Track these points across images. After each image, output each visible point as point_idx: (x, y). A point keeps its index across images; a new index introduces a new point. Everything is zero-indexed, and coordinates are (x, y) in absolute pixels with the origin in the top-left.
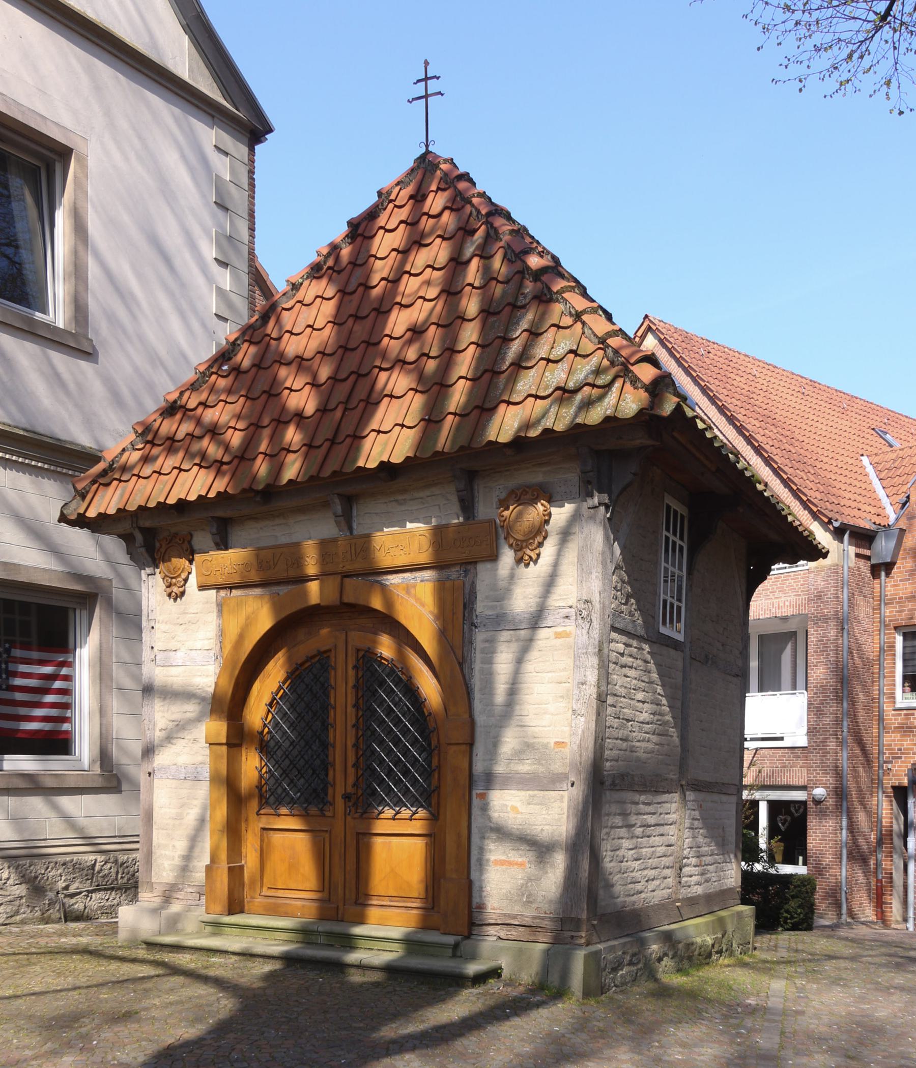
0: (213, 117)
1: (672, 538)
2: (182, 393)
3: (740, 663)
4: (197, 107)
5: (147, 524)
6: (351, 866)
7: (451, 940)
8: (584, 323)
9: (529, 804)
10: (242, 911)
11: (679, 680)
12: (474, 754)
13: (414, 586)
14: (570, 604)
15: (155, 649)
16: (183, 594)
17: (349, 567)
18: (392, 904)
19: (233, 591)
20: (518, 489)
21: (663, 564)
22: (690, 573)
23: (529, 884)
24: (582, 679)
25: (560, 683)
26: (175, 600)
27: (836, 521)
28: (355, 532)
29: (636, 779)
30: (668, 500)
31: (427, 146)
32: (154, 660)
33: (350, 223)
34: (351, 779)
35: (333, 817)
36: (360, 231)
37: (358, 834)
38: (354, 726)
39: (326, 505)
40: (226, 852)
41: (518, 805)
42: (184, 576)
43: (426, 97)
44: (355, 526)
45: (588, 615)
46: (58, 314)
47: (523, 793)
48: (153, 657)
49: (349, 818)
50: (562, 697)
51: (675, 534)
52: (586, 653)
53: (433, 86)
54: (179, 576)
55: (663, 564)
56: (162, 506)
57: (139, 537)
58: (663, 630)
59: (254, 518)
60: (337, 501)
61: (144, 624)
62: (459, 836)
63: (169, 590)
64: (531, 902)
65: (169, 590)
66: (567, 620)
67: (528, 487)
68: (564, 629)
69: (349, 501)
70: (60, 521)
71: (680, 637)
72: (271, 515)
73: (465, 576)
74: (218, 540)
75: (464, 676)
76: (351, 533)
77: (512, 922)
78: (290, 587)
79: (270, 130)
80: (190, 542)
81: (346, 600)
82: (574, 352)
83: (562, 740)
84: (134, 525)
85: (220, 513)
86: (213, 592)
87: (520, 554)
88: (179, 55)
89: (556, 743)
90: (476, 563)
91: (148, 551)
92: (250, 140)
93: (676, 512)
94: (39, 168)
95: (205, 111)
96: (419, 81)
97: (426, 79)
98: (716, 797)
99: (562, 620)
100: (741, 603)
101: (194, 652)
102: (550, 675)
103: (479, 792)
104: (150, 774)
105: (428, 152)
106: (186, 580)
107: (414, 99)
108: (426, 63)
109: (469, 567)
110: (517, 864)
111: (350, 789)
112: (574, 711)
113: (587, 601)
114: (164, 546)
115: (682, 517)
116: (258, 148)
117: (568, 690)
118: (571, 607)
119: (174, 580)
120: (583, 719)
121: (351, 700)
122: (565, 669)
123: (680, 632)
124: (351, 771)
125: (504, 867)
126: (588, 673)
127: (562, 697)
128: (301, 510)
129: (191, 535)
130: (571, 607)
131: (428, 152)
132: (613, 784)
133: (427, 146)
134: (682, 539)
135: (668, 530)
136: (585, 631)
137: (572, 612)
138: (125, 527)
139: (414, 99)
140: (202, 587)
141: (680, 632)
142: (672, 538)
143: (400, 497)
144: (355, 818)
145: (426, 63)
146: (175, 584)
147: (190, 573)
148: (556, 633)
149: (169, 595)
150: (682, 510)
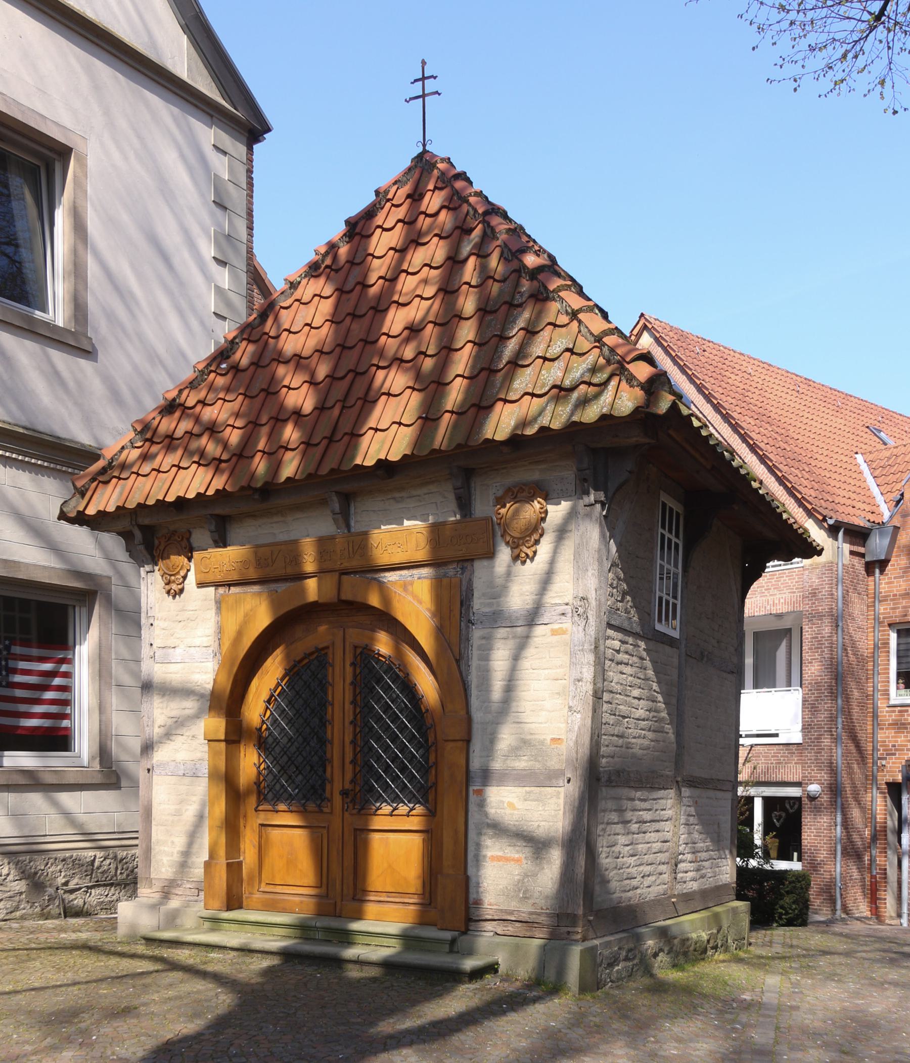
0: (212, 116)
1: (667, 535)
2: (181, 391)
5: (146, 521)
6: (349, 861)
7: (448, 935)
8: (580, 322)
9: (526, 800)
10: (240, 907)
13: (412, 583)
14: (566, 601)
15: (154, 646)
16: (181, 591)
17: (346, 565)
20: (514, 487)
21: (659, 561)
22: (685, 570)
23: (526, 880)
24: (578, 676)
26: (174, 597)
28: (353, 530)
29: (632, 775)
30: (664, 497)
31: (424, 145)
32: (153, 657)
33: (347, 222)
34: (349, 775)
35: (331, 813)
36: (357, 230)
37: (356, 830)
39: (324, 503)
43: (423, 96)
44: (352, 524)
45: (584, 612)
47: (520, 789)
48: (152, 654)
50: (558, 694)
52: (583, 650)
53: (430, 86)
54: (178, 573)
55: (659, 561)
56: (161, 503)
57: (138, 534)
58: (659, 627)
59: (252, 515)
60: (335, 498)
63: (168, 587)
65: (168, 587)
66: (563, 617)
67: (525, 484)
68: (561, 625)
69: (347, 499)
70: (59, 519)
71: (676, 634)
73: (462, 574)
74: (217, 538)
76: (349, 531)
78: (288, 584)
79: (268, 130)
80: (188, 540)
81: (343, 597)
82: (570, 350)
84: (134, 523)
85: (219, 511)
86: (213, 589)
87: (516, 551)
89: (553, 739)
90: (472, 560)
92: (248, 139)
93: (671, 510)
95: (203, 111)
96: (416, 81)
97: (424, 78)
98: (711, 793)
99: (559, 617)
102: (546, 671)
103: (475, 788)
104: (149, 770)
106: (185, 577)
107: (411, 99)
108: (424, 63)
109: (466, 564)
110: (513, 860)
111: (347, 786)
112: (570, 707)
113: (583, 599)
115: (678, 514)
118: (567, 604)
119: (173, 578)
120: (579, 716)
121: (349, 696)
122: (561, 666)
124: (349, 768)
126: (584, 670)
127: (558, 694)
129: (190, 533)
130: (567, 604)
131: (425, 151)
133: (424, 145)
134: (677, 536)
135: (663, 527)
136: (581, 628)
137: (568, 609)
138: (125, 524)
140: (201, 585)
142: (667, 535)
143: (397, 495)
145: (424, 63)
146: (174, 582)
147: (188, 570)
148: (552, 630)
149: (168, 592)
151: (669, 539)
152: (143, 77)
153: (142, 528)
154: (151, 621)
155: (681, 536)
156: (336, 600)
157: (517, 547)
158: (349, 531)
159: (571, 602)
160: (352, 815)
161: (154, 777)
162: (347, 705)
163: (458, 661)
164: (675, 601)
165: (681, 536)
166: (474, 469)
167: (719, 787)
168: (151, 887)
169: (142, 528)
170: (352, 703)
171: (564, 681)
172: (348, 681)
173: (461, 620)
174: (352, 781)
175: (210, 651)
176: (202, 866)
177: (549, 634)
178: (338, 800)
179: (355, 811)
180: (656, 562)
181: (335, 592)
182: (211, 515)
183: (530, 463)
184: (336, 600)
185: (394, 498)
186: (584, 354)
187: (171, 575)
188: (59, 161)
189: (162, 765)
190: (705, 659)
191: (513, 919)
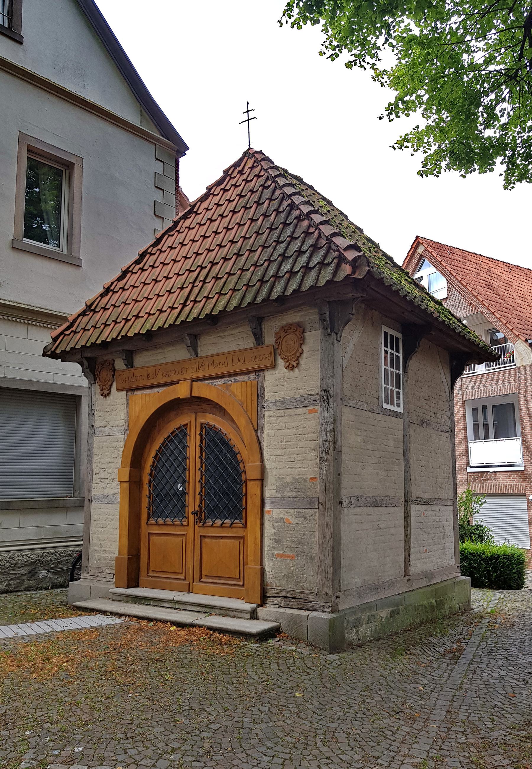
1: (390, 351)
2: (112, 283)
3: (449, 424)
5: (89, 355)
6: (197, 557)
7: (249, 607)
8: (320, 229)
10: (137, 586)
11: (401, 436)
12: (264, 486)
13: (231, 385)
14: (317, 392)
15: (95, 426)
16: (109, 394)
17: (195, 376)
18: (220, 581)
20: (286, 326)
21: (383, 367)
22: (405, 371)
23: (297, 570)
25: (313, 441)
27: (530, 339)
28: (199, 356)
29: (368, 500)
30: (385, 329)
31: (249, 145)
33: (207, 188)
34: (198, 502)
35: (188, 526)
36: (212, 192)
37: (201, 536)
38: (199, 469)
39: (182, 340)
41: (290, 518)
42: (110, 383)
44: (199, 352)
45: (327, 399)
48: (93, 431)
49: (196, 526)
50: (314, 449)
51: (392, 348)
53: (251, 115)
55: (383, 367)
56: (93, 345)
57: (86, 363)
58: (385, 406)
59: (146, 349)
60: (187, 338)
62: (255, 538)
64: (299, 582)
65: (102, 392)
66: (315, 402)
67: (291, 325)
68: (314, 407)
69: (195, 337)
71: (400, 410)
72: (155, 347)
73: (258, 378)
74: (127, 363)
75: (258, 437)
76: (197, 356)
77: (288, 595)
78: (165, 388)
79: (188, 149)
80: (113, 365)
81: (193, 395)
83: (314, 477)
85: (126, 347)
86: (125, 392)
87: (288, 364)
88: (130, 113)
89: (311, 478)
90: (264, 370)
91: (90, 371)
93: (392, 336)
97: (248, 111)
98: (436, 508)
99: (312, 402)
100: (447, 388)
101: (114, 427)
104: (89, 500)
105: (250, 148)
109: (261, 373)
110: (290, 557)
111: (197, 509)
114: (100, 367)
115: (397, 339)
117: (317, 445)
121: (198, 454)
122: (315, 432)
123: (400, 406)
124: (198, 497)
125: (282, 558)
127: (314, 449)
128: (171, 344)
129: (114, 361)
130: (317, 394)
131: (250, 148)
132: (350, 503)
133: (249, 145)
134: (398, 351)
135: (386, 346)
136: (325, 409)
137: (318, 397)
138: (78, 356)
140: (119, 390)
141: (400, 406)
142: (390, 351)
143: (222, 334)
144: (199, 527)
147: (112, 382)
150: (397, 334)
151: (398, 352)
153: (87, 359)
154: (93, 412)
155: (401, 351)
156: (189, 396)
157: (288, 361)
158: (197, 356)
160: (199, 527)
161: (92, 504)
162: (197, 457)
163: (256, 431)
164: (398, 390)
165: (401, 351)
166: (264, 317)
167: (441, 504)
168: (88, 573)
169: (87, 359)
170: (200, 457)
172: (198, 444)
173: (258, 406)
174: (199, 506)
175: (123, 429)
176: (115, 559)
177: (308, 413)
178: (191, 517)
179: (201, 524)
180: (381, 367)
181: (189, 392)
182: (123, 350)
183: (294, 312)
184: (189, 396)
187: (103, 386)
189: (98, 497)
190: (425, 424)
191: (291, 596)
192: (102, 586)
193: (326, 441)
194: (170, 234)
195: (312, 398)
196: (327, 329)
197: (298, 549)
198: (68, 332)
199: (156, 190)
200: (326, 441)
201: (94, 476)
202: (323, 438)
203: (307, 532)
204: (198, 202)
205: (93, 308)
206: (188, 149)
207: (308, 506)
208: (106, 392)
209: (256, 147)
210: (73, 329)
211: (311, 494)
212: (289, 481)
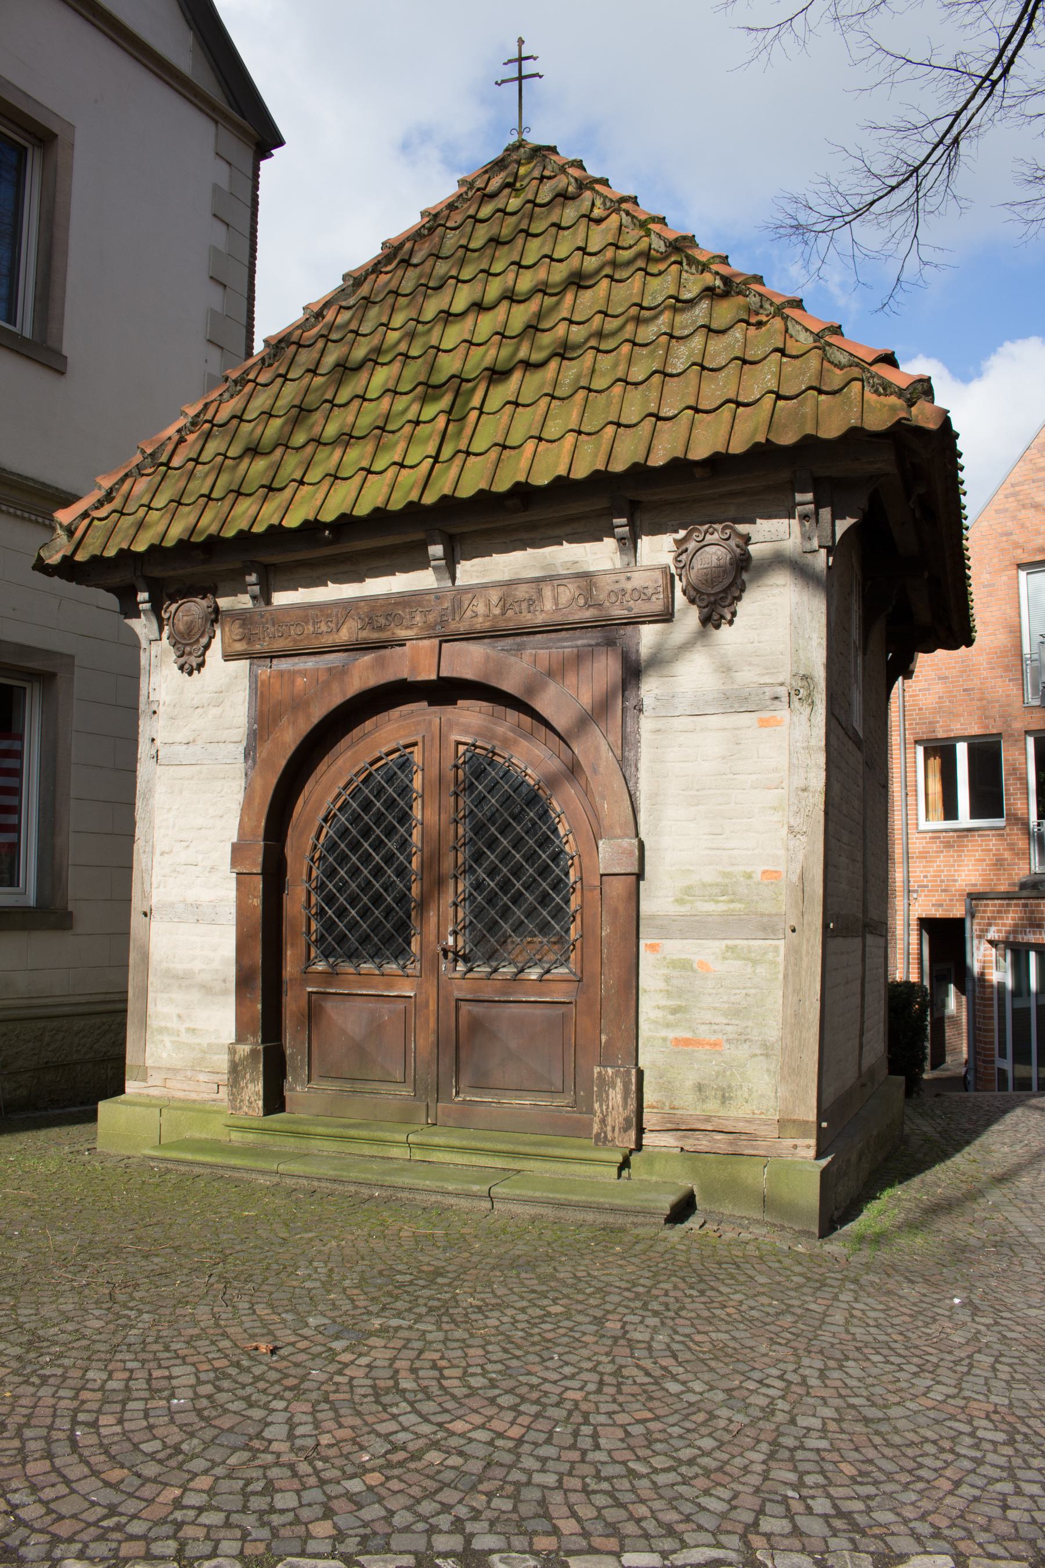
0: (216, 122)
4: (200, 109)
9: (724, 958)
14: (781, 680)
15: (158, 742)
16: (201, 665)
19: (275, 661)
24: (802, 784)
26: (190, 674)
32: (156, 757)
40: (929, 1176)
42: (204, 641)
43: (521, 78)
44: (458, 575)
46: (25, 326)
47: (717, 943)
48: (154, 752)
52: (808, 748)
53: (528, 67)
61: (142, 706)
63: (182, 660)
65: (182, 660)
66: (776, 702)
70: (34, 568)
76: (1020, 566)
79: (280, 142)
82: (782, 351)
84: (139, 573)
86: (245, 664)
89: (764, 872)
92: (255, 152)
94: (26, 149)
95: (208, 115)
96: (510, 61)
97: (521, 59)
103: (649, 942)
104: (145, 914)
106: (207, 647)
107: (503, 82)
108: (521, 42)
112: (790, 827)
113: (805, 677)
116: (263, 164)
118: (782, 684)
119: (188, 649)
120: (804, 839)
126: (811, 775)
130: (782, 684)
136: (804, 718)
137: (782, 691)
139: (503, 82)
140: (228, 657)
145: (521, 42)
146: (190, 654)
147: (211, 638)
148: (761, 720)
149: (181, 668)
152: (143, 68)
154: (154, 707)
159: (788, 682)
168: (145, 1080)
171: (780, 790)
185: (521, 540)
186: (635, 425)
188: (38, 154)
192: (518, 1192)
193: (804, 790)
194: (344, 304)
195: (769, 692)
196: (810, 539)
197: (729, 1028)
198: (102, 513)
199: (215, 220)
200: (804, 790)
201: (157, 857)
202: (799, 782)
203: (753, 991)
204: (408, 239)
205: (164, 459)
206: (280, 142)
207: (760, 934)
208: (194, 661)
209: (536, 138)
210: (117, 503)
211: (766, 907)
212: (708, 879)
